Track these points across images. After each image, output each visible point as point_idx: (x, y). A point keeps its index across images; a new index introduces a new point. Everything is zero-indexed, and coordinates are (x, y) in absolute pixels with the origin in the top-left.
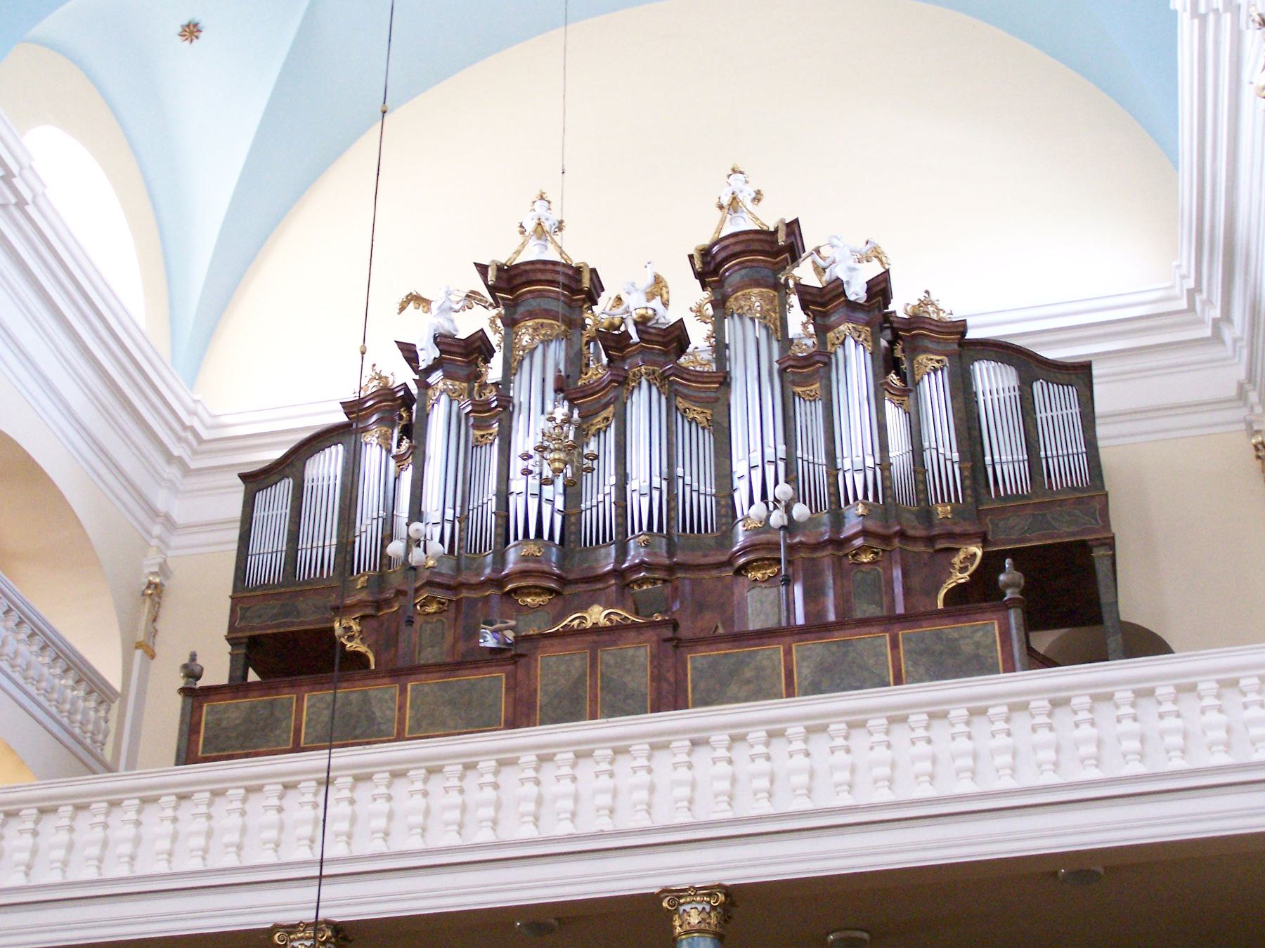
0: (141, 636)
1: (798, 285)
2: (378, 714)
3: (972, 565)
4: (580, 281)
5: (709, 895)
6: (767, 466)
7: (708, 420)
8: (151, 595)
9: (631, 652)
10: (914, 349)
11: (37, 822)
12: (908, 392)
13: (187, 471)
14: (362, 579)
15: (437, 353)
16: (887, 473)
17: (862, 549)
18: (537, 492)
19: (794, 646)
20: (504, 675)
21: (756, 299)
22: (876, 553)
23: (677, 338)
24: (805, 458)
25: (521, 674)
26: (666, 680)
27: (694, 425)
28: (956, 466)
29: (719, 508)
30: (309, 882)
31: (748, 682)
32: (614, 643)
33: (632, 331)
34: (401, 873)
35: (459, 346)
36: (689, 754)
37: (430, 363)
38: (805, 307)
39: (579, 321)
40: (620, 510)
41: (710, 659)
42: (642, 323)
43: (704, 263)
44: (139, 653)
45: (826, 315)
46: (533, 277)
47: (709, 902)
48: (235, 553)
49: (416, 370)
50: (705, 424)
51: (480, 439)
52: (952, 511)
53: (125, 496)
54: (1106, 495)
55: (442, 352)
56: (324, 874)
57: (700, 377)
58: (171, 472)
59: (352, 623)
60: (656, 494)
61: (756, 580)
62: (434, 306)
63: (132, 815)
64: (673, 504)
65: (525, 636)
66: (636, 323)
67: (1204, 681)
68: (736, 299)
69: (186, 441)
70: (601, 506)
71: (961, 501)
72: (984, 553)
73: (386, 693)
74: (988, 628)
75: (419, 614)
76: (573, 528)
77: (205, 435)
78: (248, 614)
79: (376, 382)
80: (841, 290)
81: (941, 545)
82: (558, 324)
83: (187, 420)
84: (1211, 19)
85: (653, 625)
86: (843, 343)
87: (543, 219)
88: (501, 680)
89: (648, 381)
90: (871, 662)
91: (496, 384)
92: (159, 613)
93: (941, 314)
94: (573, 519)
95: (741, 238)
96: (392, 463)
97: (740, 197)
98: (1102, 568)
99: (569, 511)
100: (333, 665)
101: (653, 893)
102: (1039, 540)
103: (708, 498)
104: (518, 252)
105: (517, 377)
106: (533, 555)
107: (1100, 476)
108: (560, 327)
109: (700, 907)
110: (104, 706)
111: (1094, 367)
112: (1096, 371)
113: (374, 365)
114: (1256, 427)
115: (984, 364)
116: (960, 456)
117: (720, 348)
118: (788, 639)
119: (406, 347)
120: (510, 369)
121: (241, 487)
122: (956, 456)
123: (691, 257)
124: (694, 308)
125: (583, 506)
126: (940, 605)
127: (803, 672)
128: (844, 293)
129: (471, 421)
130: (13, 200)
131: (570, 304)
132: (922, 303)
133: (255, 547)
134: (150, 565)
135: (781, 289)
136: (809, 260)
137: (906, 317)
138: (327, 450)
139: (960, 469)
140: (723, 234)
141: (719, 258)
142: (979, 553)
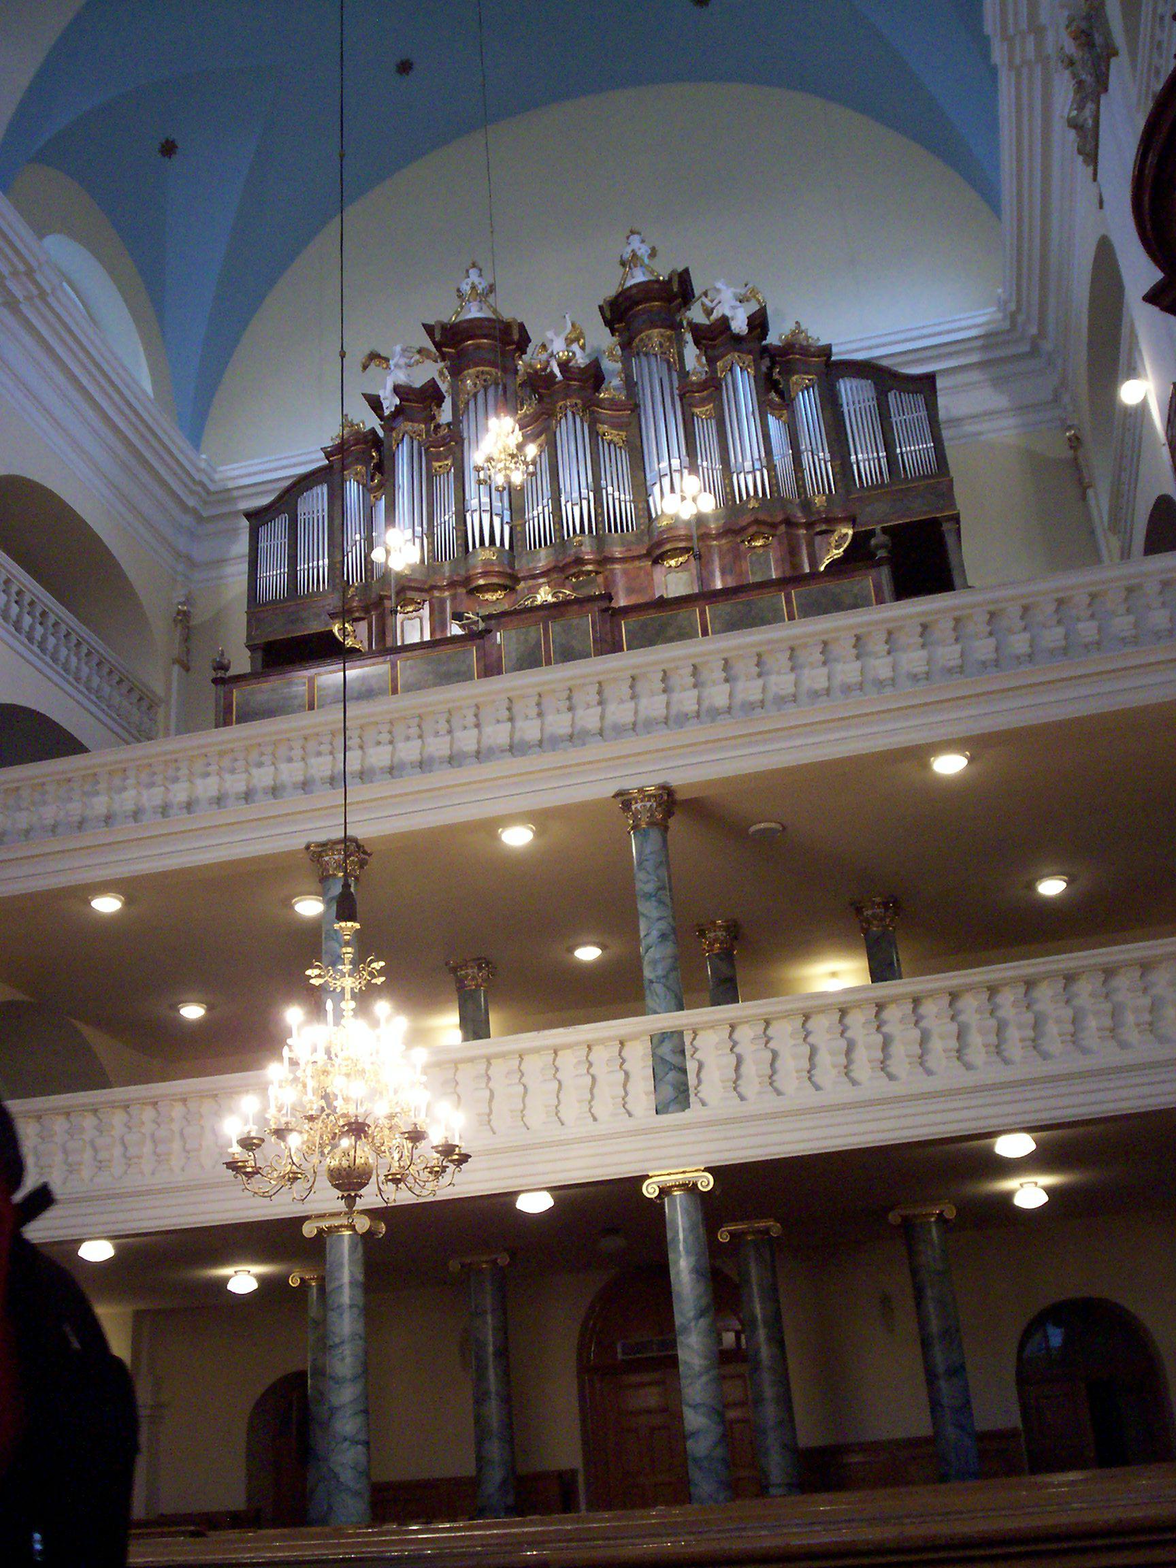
1: (689, 323)
6: (674, 474)
8: (181, 620)
10: (788, 371)
12: (786, 404)
21: (656, 336)
27: (612, 446)
32: (562, 615)
38: (697, 343)
42: (563, 366)
49: (381, 417)
50: (621, 444)
54: (951, 481)
55: (401, 400)
60: (585, 503)
66: (559, 365)
69: (197, 493)
70: (541, 516)
72: (854, 534)
83: (198, 476)
84: (1025, 70)
85: (591, 599)
86: (731, 370)
89: (573, 412)
91: (449, 425)
94: (519, 529)
97: (639, 253)
98: (950, 540)
99: (515, 523)
102: (899, 518)
103: (628, 504)
105: (465, 417)
107: (946, 464)
112: (940, 383)
114: (1069, 423)
117: (630, 385)
123: (601, 308)
128: (728, 328)
130: (36, 292)
132: (793, 334)
134: (179, 595)
135: (676, 326)
136: (699, 303)
142: (850, 532)
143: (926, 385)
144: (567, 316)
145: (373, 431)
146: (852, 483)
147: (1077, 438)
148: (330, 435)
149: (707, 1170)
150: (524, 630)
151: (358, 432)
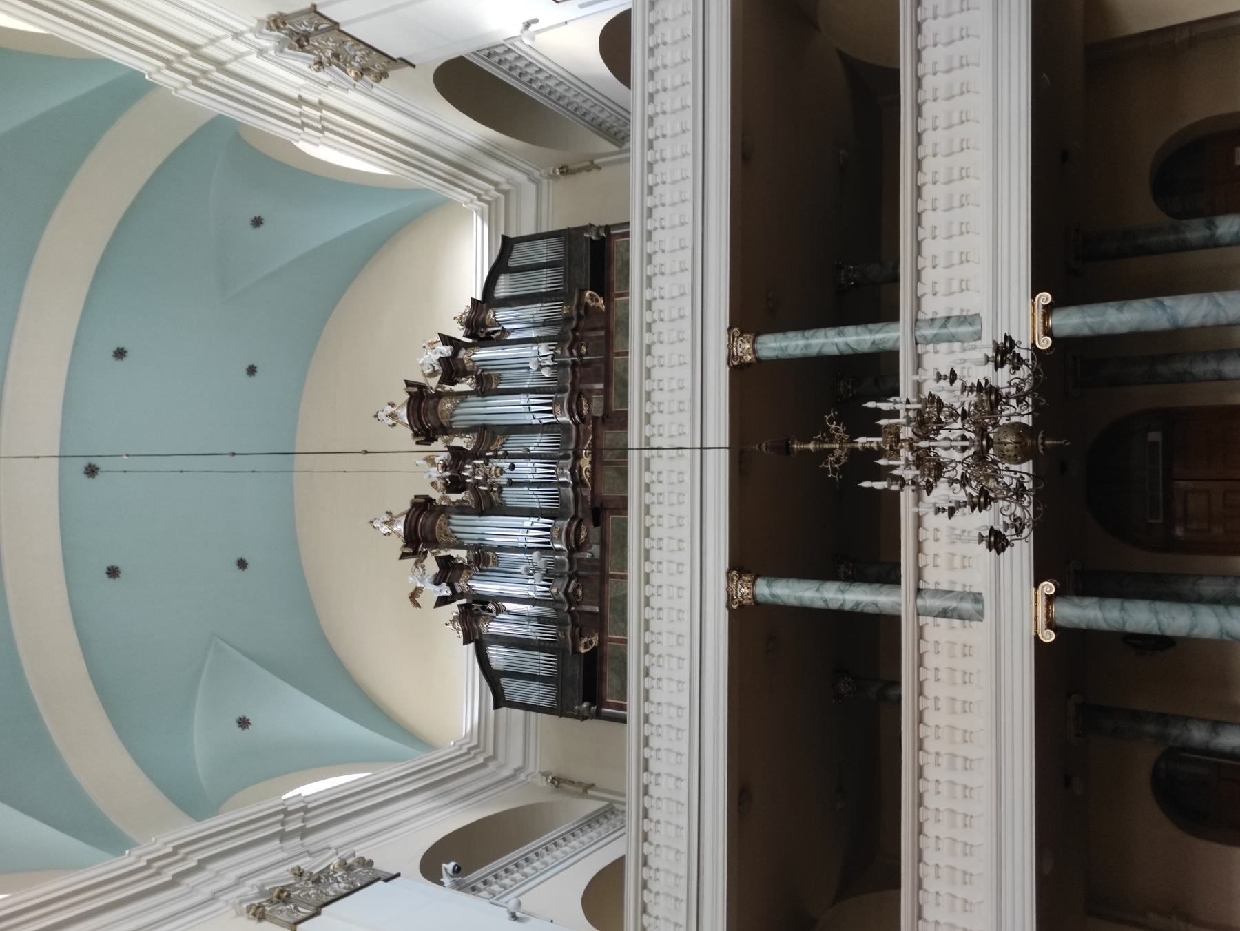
0: (580, 790)
4: (420, 503)
5: (733, 338)
8: (558, 782)
11: (652, 773)
13: (493, 758)
14: (560, 635)
15: (444, 584)
16: (542, 339)
19: (615, 351)
20: (611, 517)
22: (582, 344)
25: (612, 506)
27: (504, 445)
28: (544, 305)
35: (443, 573)
36: (654, 357)
37: (448, 588)
40: (542, 485)
43: (422, 435)
44: (590, 792)
45: (458, 372)
46: (413, 528)
47: (738, 338)
52: (566, 306)
53: (500, 788)
55: (444, 581)
56: (699, 446)
57: (480, 440)
58: (492, 766)
59: (583, 642)
62: (419, 585)
64: (543, 456)
68: (442, 418)
69: (476, 754)
74: (619, 244)
76: (548, 512)
77: (475, 743)
80: (445, 359)
81: (582, 312)
83: (464, 750)
85: (594, 429)
87: (383, 521)
88: (614, 518)
92: (570, 779)
94: (544, 512)
95: (410, 412)
96: (501, 616)
97: (389, 412)
100: (623, 704)
101: (730, 371)
104: (399, 535)
105: (465, 541)
108: (442, 517)
109: (740, 342)
110: (615, 812)
113: (446, 624)
114: (551, 173)
115: (496, 291)
118: (611, 354)
119: (438, 603)
120: (460, 546)
121: (503, 710)
125: (538, 507)
128: (447, 358)
129: (485, 568)
130: (302, 814)
131: (432, 511)
133: (535, 701)
135: (439, 395)
138: (489, 656)
139: (545, 303)
140: (407, 422)
141: (420, 426)
143: (508, 244)
144: (417, 463)
147: (562, 168)
148: (455, 635)
149: (1036, 586)
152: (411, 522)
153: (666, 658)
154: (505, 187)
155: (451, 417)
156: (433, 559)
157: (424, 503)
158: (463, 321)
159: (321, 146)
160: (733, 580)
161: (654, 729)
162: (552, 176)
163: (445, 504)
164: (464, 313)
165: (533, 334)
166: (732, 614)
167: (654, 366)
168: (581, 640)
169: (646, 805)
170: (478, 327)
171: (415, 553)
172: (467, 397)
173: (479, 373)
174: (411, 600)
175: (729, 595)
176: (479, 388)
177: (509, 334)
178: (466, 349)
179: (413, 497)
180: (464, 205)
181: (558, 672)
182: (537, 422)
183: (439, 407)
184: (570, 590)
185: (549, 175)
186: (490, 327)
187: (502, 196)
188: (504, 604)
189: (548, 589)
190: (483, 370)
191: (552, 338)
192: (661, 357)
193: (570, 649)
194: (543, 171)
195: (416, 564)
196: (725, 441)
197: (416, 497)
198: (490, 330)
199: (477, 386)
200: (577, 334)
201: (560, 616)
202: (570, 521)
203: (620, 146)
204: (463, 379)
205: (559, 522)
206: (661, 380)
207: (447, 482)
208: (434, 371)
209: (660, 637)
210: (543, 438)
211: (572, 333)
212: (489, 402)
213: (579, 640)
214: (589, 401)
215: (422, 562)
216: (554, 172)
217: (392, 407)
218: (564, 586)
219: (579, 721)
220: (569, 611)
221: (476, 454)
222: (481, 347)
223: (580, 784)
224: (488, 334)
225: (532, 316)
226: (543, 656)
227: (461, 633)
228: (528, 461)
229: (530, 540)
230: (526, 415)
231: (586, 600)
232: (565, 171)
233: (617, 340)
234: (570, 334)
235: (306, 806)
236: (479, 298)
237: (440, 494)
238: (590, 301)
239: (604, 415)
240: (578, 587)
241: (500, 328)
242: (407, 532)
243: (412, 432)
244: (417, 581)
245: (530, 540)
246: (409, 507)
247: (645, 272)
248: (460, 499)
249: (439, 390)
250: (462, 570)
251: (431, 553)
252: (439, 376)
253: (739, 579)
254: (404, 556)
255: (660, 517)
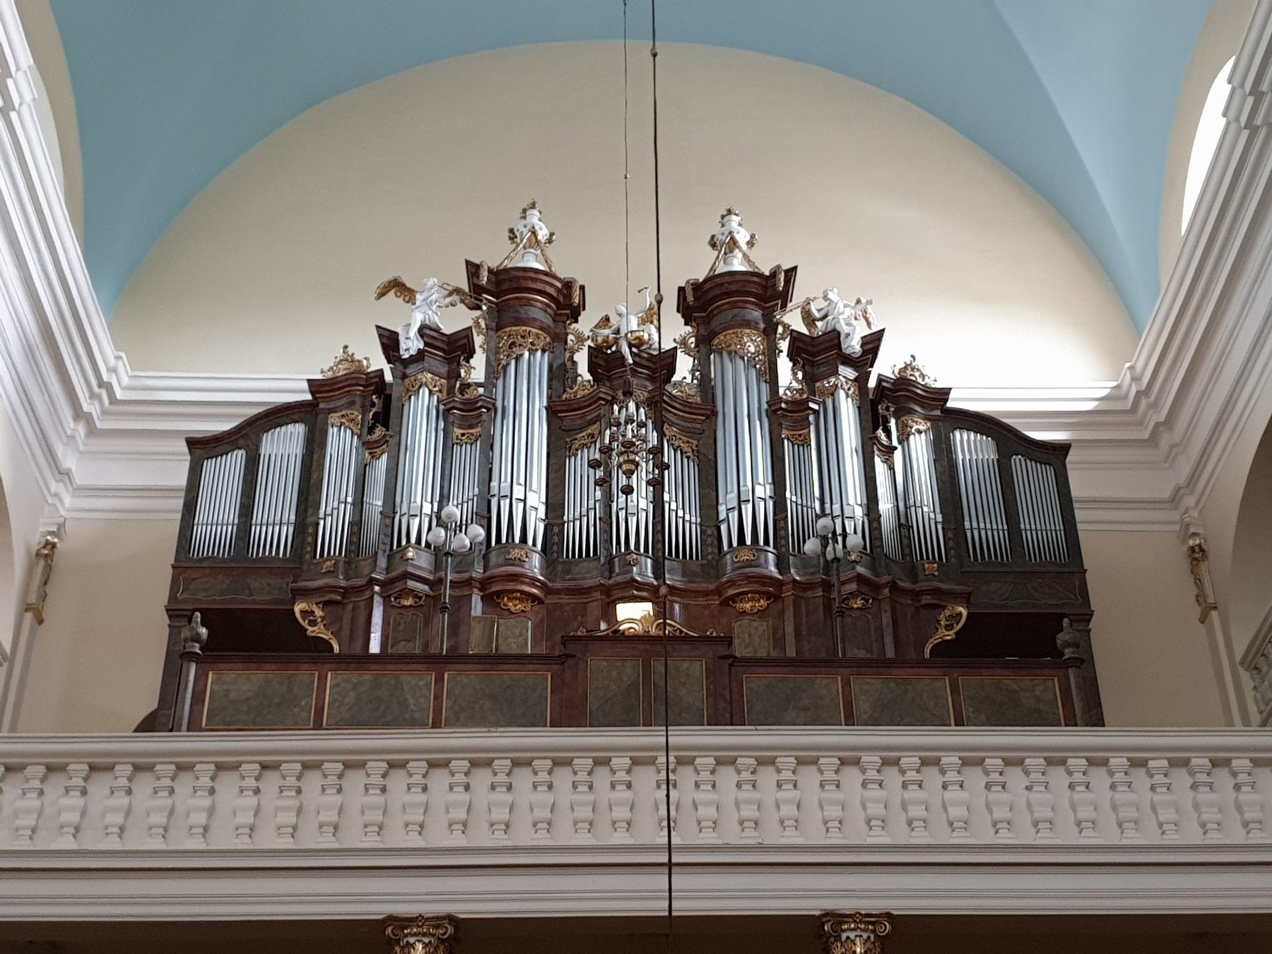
0: (33, 599)
2: (411, 701)
3: (957, 623)
5: (873, 923)
7: (693, 451)
9: (686, 665)
13: (92, 431)
14: (328, 563)
16: (875, 525)
17: (853, 595)
18: (523, 498)
22: (867, 601)
23: (664, 363)
24: (799, 502)
26: (723, 697)
28: (940, 527)
29: (704, 537)
30: (659, 869)
31: (806, 709)
33: (625, 350)
34: (1103, 869)
37: (413, 352)
39: (563, 336)
41: (766, 681)
44: (29, 616)
47: (873, 931)
48: (179, 523)
51: (460, 437)
55: (426, 344)
56: (674, 860)
57: (686, 405)
59: (315, 608)
61: (745, 611)
63: (205, 781)
65: (573, 636)
66: (630, 345)
67: (1239, 758)
71: (944, 561)
73: (421, 680)
74: (1049, 684)
75: (393, 606)
76: (556, 539)
78: (192, 586)
79: (346, 365)
81: (926, 600)
82: (545, 335)
85: (710, 639)
87: (537, 228)
90: (932, 703)
93: (927, 380)
94: (556, 530)
95: (738, 278)
97: (737, 237)
106: (519, 559)
108: (545, 339)
109: (865, 935)
111: (1071, 452)
113: (346, 347)
114: (1192, 530)
116: (943, 517)
118: (846, 671)
119: (386, 333)
120: (495, 371)
122: (939, 518)
123: (681, 290)
124: (677, 340)
125: (565, 518)
126: (927, 655)
127: (862, 705)
128: (840, 347)
133: (201, 516)
135: (769, 331)
137: (892, 377)
139: (943, 529)
141: (711, 295)
142: (965, 613)
143: (1055, 454)
145: (380, 373)
146: (965, 554)
147: (1202, 550)
148: (321, 365)
150: (619, 664)
151: (360, 372)
152: (536, 280)
153: (295, 803)
154: (1166, 440)
155: (729, 353)
156: (469, 323)
157: (571, 305)
158: (909, 372)
159: (1224, 120)
160: (437, 927)
161: (166, 782)
162: (1186, 532)
163: (569, 342)
164: (923, 376)
165: (885, 506)
166: (377, 926)
167: (822, 772)
168: (317, 604)
169: (29, 768)
170: (895, 400)
171: (477, 289)
172: (766, 381)
173: (812, 405)
174: (390, 282)
175: (411, 920)
176: (783, 405)
177: (885, 461)
178: (856, 380)
179: (581, 283)
180: (1128, 365)
181: (258, 560)
182: (722, 516)
183: (748, 331)
184: (411, 584)
185: (1188, 525)
186: (897, 424)
187: (1146, 435)
188: (385, 456)
189: (413, 540)
190: (816, 412)
191: (878, 543)
192: (838, 786)
193: (301, 584)
194: (1195, 514)
195: (457, 291)
196: (682, 907)
197: (582, 288)
198: (893, 422)
199: (787, 402)
200: (886, 591)
201: (363, 563)
202: (539, 580)
203: (1242, 663)
204: (800, 375)
205: (536, 560)
206: (795, 786)
207: (610, 348)
208: (815, 320)
209: (334, 791)
210: (694, 526)
211: (889, 582)
212: (758, 423)
213: (318, 600)
214: (761, 614)
215: (462, 301)
216: (1194, 535)
217: (748, 243)
218: (418, 573)
219: (166, 602)
220: (372, 582)
221: (658, 406)
222: (859, 408)
223: (44, 597)
224: (886, 421)
225: (918, 504)
226: (287, 531)
227: (330, 374)
228: (651, 498)
229: (505, 504)
230: (735, 494)
231: (394, 612)
232: (1197, 555)
233: (867, 688)
234: (885, 579)
235: (14, 110)
236: (950, 404)
237: (587, 333)
238: (947, 613)
239: (735, 657)
240: (417, 596)
241: (895, 443)
242: (516, 273)
243: (701, 280)
244: (425, 295)
245: (505, 504)
246: (562, 274)
247: (990, 754)
248: (579, 372)
249: (780, 329)
250: (448, 378)
251: (478, 318)
252: (804, 331)
253: (439, 939)
254: (473, 269)
255: (550, 787)
